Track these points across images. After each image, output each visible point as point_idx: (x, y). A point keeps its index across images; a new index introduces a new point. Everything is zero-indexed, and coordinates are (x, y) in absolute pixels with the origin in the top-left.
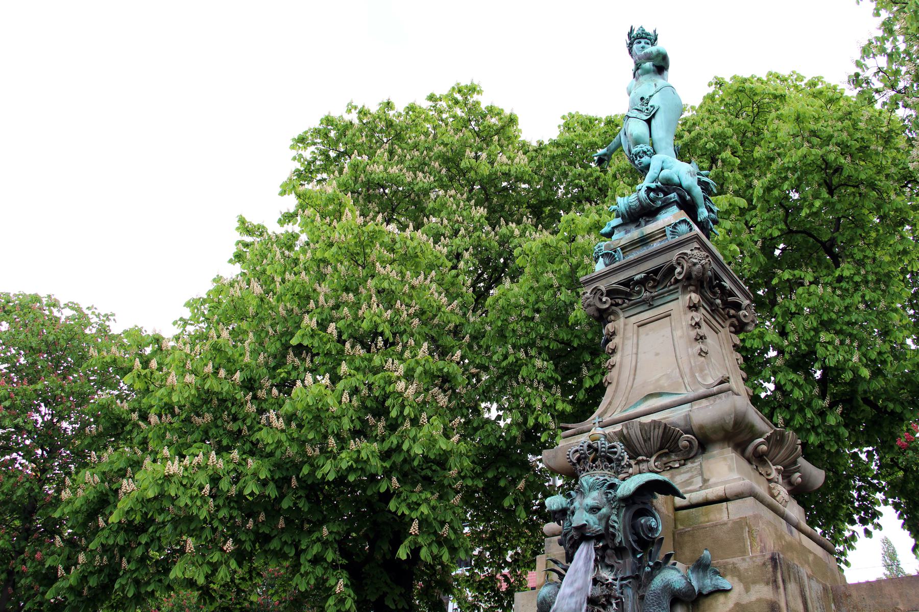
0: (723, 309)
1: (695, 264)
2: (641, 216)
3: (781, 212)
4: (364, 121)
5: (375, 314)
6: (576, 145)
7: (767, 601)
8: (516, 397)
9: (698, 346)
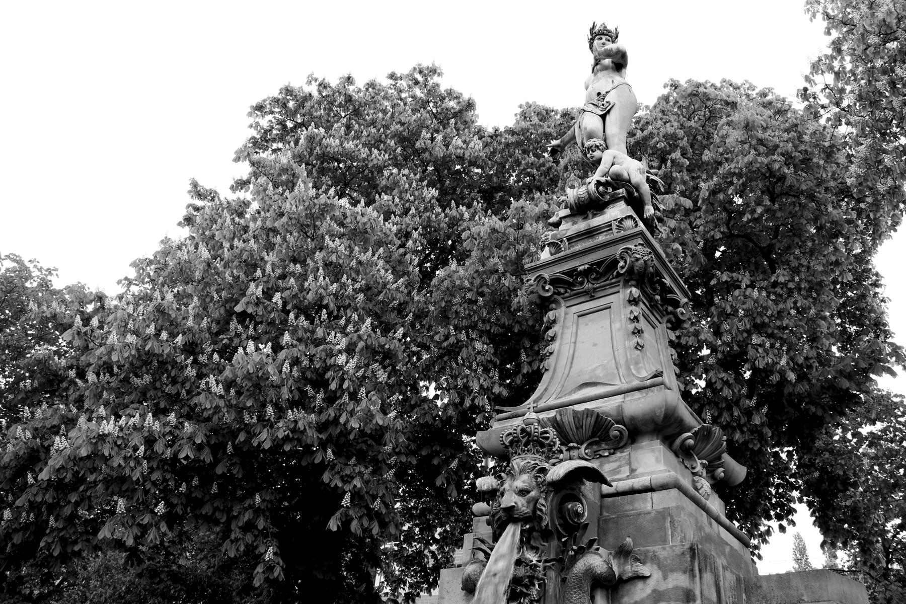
0: (662, 306)
1: (638, 260)
4: (324, 94)
5: (321, 286)
6: (531, 134)
7: (683, 589)
8: (455, 377)
9: (635, 339)
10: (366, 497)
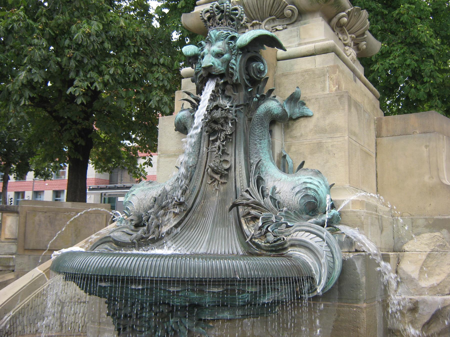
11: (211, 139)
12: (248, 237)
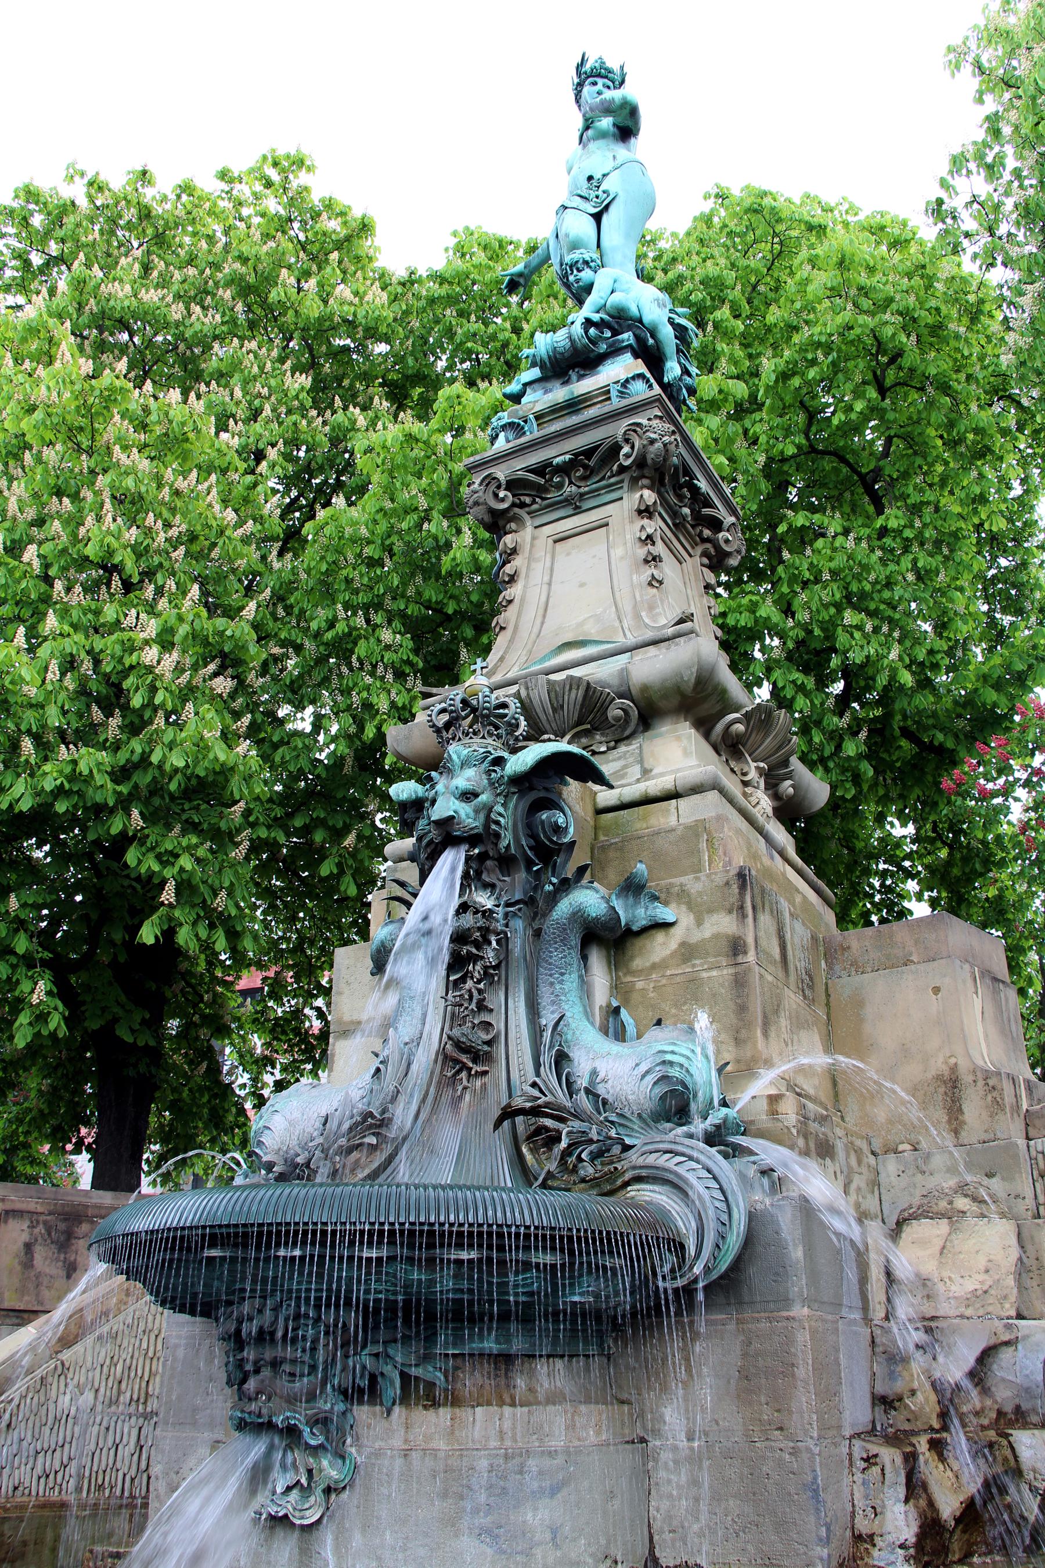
0: (693, 527)
1: (652, 442)
2: (573, 367)
3: (801, 418)
4: (99, 203)
5: (109, 532)
6: (474, 284)
7: (727, 936)
8: (346, 692)
9: (649, 571)
10: (202, 888)
11: (452, 978)
12: (536, 1179)
